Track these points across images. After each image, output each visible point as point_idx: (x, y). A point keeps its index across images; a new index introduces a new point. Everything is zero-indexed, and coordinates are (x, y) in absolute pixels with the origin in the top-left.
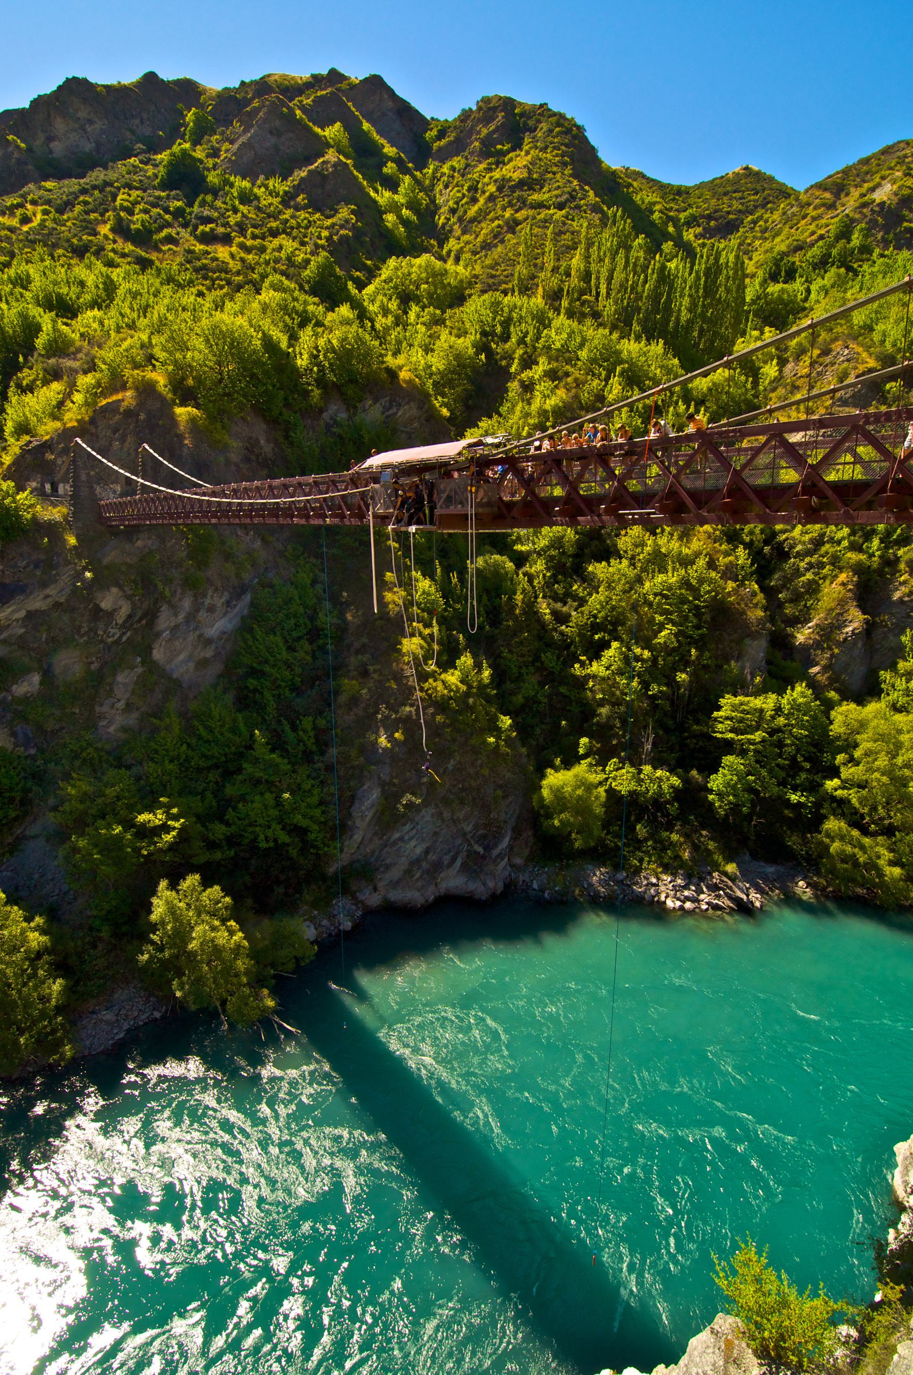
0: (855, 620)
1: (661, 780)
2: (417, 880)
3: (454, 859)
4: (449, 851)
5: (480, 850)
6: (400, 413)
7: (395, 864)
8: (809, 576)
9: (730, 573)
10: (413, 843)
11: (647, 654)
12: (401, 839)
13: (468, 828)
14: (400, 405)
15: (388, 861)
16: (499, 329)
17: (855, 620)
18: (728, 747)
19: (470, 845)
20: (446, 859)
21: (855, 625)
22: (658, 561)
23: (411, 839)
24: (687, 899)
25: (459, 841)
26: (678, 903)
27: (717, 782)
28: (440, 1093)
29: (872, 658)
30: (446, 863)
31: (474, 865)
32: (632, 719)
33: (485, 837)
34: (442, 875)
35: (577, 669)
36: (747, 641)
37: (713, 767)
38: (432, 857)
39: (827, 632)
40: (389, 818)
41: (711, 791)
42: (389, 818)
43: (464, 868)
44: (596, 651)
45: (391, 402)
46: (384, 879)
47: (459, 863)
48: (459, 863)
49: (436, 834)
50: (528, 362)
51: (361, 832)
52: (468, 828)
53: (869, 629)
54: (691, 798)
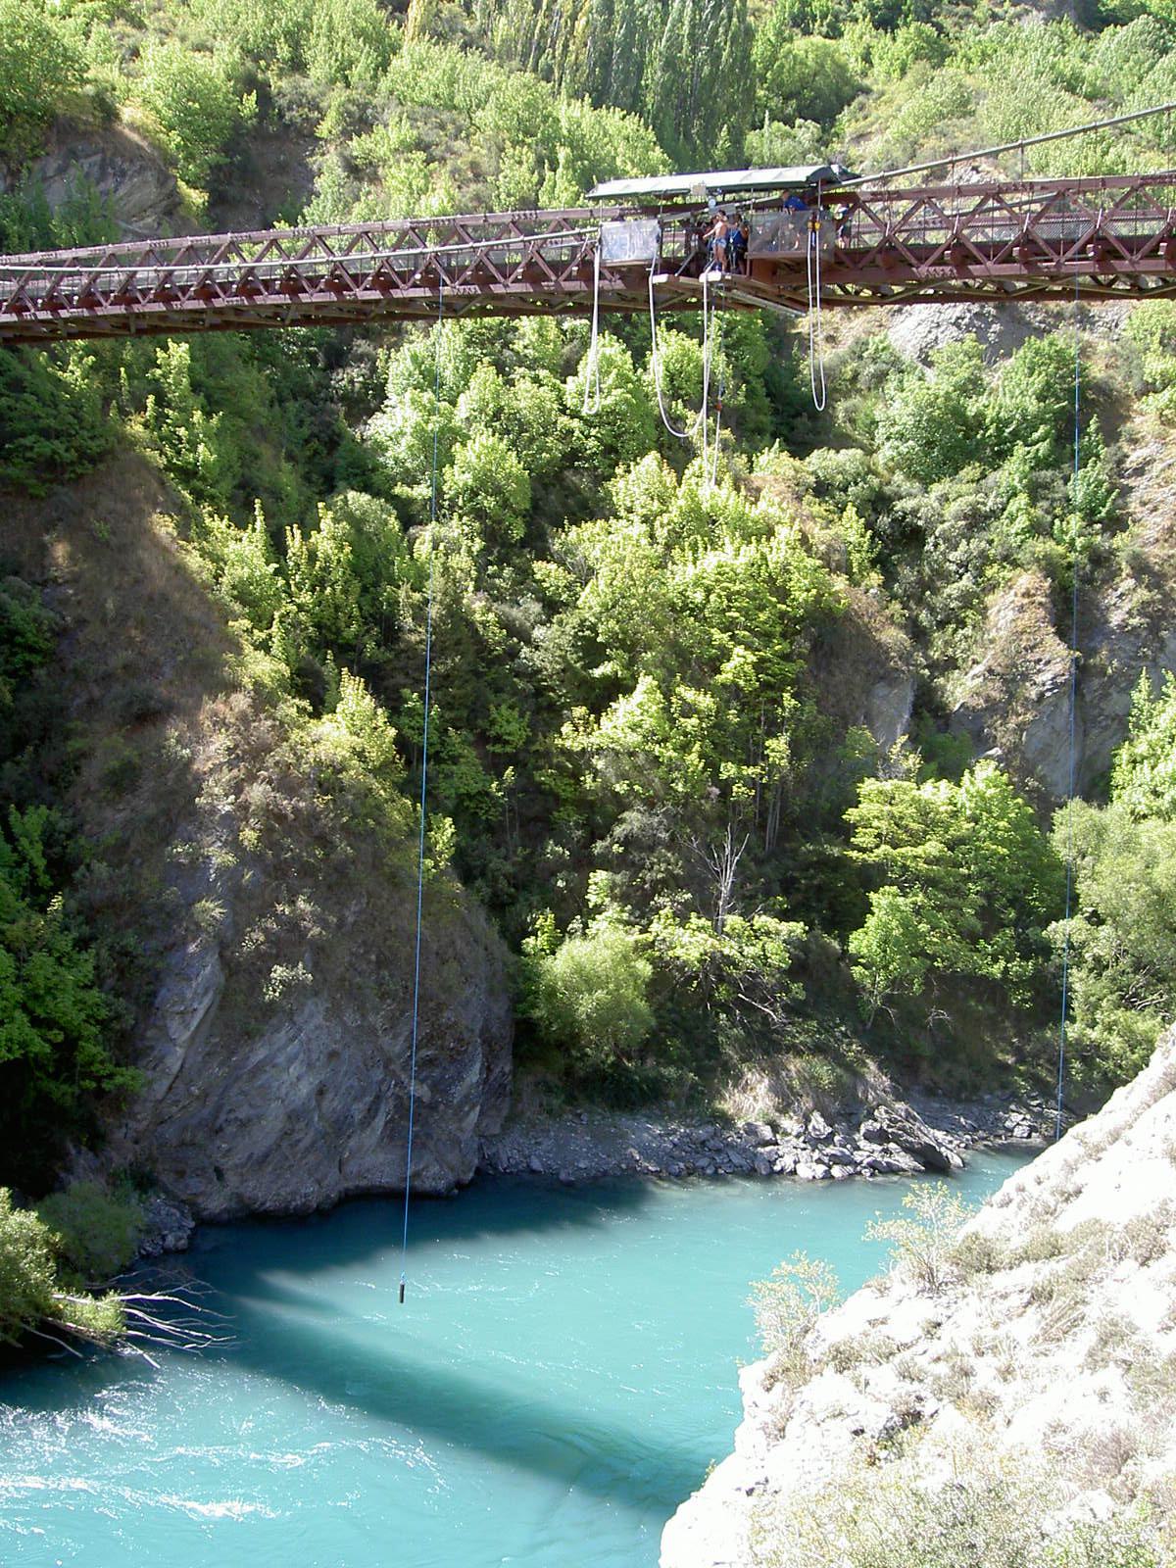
0: (1055, 660)
1: (769, 939)
2: (307, 1150)
3: (372, 1112)
4: (364, 1092)
5: (423, 1091)
6: (121, 192)
7: (259, 1117)
8: (966, 582)
9: (836, 561)
10: (294, 1070)
11: (706, 702)
12: (269, 1061)
13: (396, 1047)
14: (123, 174)
15: (242, 1114)
16: (284, 51)
17: (1055, 660)
18: (873, 877)
19: (400, 1084)
20: (358, 1110)
21: (1057, 668)
22: (703, 525)
23: (291, 1061)
24: (836, 1160)
25: (378, 1074)
26: (821, 1169)
27: (861, 942)
28: (648, 1159)
29: (1086, 734)
30: (358, 1117)
31: (412, 1123)
32: (702, 818)
33: (430, 1062)
34: (352, 1143)
35: (570, 738)
36: (881, 690)
37: (852, 916)
38: (332, 1103)
39: (1012, 678)
40: (242, 1013)
41: (854, 960)
42: (242, 1013)
43: (392, 1133)
44: (601, 697)
45: (103, 167)
46: (234, 1151)
47: (380, 1122)
48: (380, 1122)
49: (333, 1055)
50: (360, 122)
51: (180, 1051)
52: (396, 1047)
53: (1082, 672)
54: (818, 976)
